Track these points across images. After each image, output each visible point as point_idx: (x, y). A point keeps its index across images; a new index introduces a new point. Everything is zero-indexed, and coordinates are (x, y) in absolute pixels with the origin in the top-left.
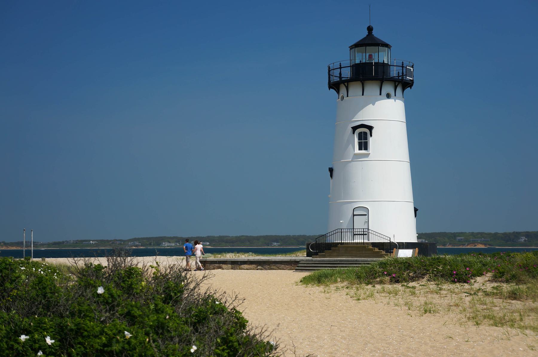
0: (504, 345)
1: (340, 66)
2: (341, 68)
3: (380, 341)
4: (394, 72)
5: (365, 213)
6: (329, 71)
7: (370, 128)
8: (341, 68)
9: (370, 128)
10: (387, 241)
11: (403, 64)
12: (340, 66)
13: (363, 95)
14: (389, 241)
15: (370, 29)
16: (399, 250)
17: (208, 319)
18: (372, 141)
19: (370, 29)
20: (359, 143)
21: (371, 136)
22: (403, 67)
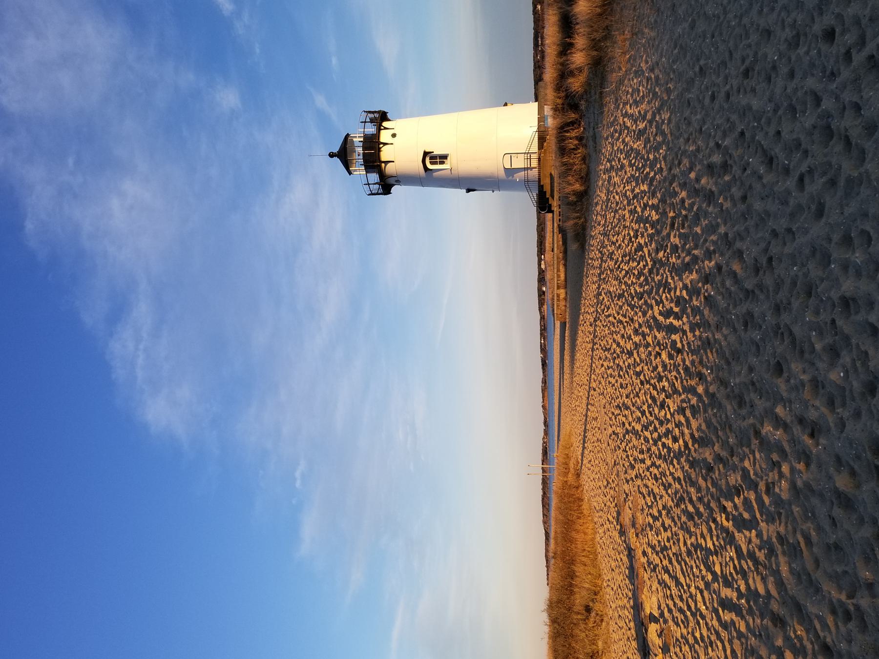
2: (369, 184)
4: (371, 129)
7: (426, 154)
8: (369, 184)
9: (426, 154)
13: (393, 162)
15: (332, 155)
18: (437, 152)
21: (433, 152)
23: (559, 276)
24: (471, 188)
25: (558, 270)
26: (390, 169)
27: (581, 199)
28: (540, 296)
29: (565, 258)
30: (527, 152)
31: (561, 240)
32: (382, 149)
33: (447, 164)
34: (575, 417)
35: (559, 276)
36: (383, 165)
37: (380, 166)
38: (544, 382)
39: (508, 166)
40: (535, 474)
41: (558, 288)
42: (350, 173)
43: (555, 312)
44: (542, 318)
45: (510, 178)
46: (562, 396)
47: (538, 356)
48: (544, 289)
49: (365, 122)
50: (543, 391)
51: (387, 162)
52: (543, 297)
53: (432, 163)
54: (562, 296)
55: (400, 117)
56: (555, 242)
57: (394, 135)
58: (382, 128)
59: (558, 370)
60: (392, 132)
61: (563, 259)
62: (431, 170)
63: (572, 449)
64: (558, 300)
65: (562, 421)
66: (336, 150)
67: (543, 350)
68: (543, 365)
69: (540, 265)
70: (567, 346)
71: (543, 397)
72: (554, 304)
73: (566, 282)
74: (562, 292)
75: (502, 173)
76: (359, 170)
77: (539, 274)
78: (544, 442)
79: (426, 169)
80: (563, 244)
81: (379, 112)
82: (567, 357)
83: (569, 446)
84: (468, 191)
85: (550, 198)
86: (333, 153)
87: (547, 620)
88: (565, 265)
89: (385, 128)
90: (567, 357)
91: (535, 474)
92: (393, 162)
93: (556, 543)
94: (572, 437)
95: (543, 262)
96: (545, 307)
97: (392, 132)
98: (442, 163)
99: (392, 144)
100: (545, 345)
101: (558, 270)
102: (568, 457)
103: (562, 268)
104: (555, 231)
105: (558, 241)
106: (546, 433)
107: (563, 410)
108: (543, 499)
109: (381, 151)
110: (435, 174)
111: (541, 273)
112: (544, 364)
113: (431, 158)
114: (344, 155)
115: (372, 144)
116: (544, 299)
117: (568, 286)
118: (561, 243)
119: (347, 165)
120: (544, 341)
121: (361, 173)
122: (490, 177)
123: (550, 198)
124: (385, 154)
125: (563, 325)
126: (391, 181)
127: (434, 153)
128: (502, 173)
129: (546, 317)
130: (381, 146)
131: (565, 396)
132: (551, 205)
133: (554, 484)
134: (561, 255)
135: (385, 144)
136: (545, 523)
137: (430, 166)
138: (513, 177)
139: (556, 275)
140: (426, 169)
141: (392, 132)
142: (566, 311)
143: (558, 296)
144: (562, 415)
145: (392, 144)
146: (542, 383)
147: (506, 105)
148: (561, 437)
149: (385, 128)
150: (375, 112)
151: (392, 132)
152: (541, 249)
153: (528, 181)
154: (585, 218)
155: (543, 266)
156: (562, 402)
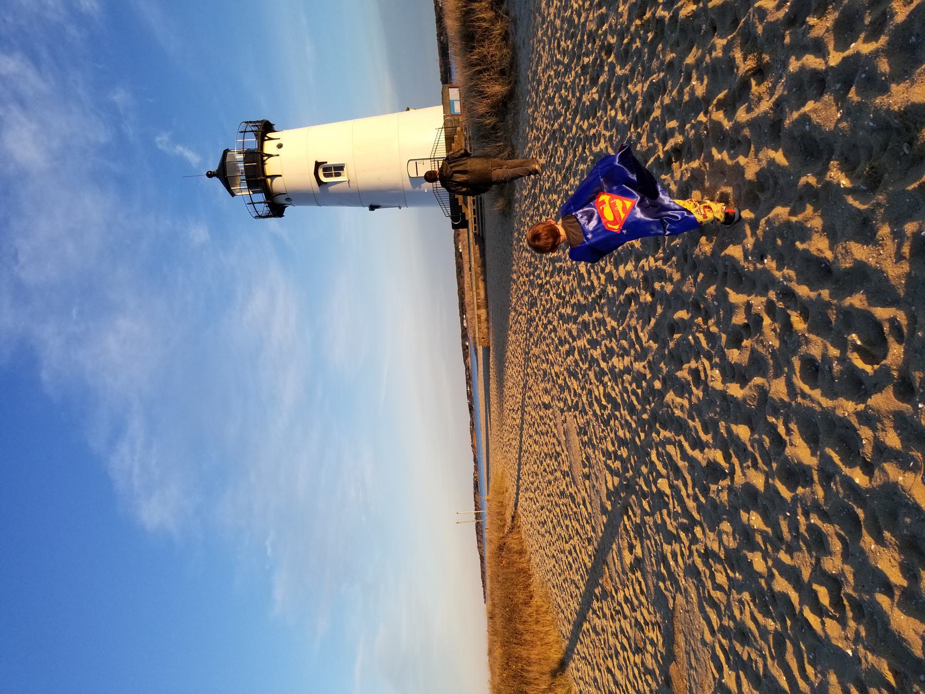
0: (697, 420)
1: (250, 204)
2: (253, 203)
3: (497, 89)
4: (251, 142)
5: (851, 248)
6: (260, 217)
7: (318, 165)
8: (253, 203)
9: (318, 165)
10: (443, 132)
11: (242, 132)
12: (250, 204)
13: (281, 176)
14: (443, 129)
15: (210, 175)
16: (437, 105)
17: (910, 76)
18: (331, 162)
19: (210, 175)
20: (336, 176)
21: (326, 162)
22: (245, 132)
23: (478, 294)
24: (374, 203)
25: (477, 288)
26: (277, 185)
27: (504, 118)
28: (464, 350)
29: (484, 273)
30: (433, 157)
31: (478, 252)
32: (266, 162)
33: (344, 176)
34: (509, 455)
35: (478, 294)
36: (269, 180)
37: (266, 182)
38: (472, 424)
39: (413, 175)
40: (465, 522)
41: (479, 307)
42: (233, 195)
43: (477, 336)
44: (467, 369)
45: (417, 189)
46: (489, 432)
47: (466, 402)
48: (467, 344)
49: (245, 132)
50: (472, 432)
51: (273, 177)
52: (467, 350)
53: (326, 176)
54: (483, 317)
55: (287, 127)
56: (472, 254)
57: (280, 146)
58: (266, 138)
59: (484, 408)
60: (277, 142)
61: (482, 274)
62: (326, 183)
63: (507, 495)
64: (479, 322)
65: (491, 459)
66: (214, 168)
67: (470, 396)
68: (470, 410)
69: (462, 323)
70: (492, 373)
71: (472, 438)
72: (476, 343)
73: (487, 300)
74: (483, 312)
75: (407, 184)
76: (243, 191)
77: (462, 331)
78: (475, 477)
79: (320, 182)
80: (481, 257)
81: (262, 121)
82: (493, 386)
83: (501, 492)
84: (372, 208)
85: (463, 206)
86: (211, 172)
87: (490, 686)
88: (485, 280)
89: (270, 139)
90: (493, 386)
91: (465, 522)
92: (281, 176)
93: (492, 582)
94: (506, 479)
95: (465, 321)
96: (469, 359)
97: (277, 142)
98: (338, 175)
99: (278, 155)
100: (471, 392)
101: (477, 288)
102: (502, 505)
103: (481, 285)
104: (471, 241)
105: (475, 254)
106: (476, 468)
107: (492, 447)
108: (477, 527)
109: (265, 164)
110: (331, 188)
111: (464, 330)
112: (471, 409)
113: (325, 170)
114: (223, 173)
115: (256, 159)
116: (468, 353)
117: (490, 303)
118: (478, 255)
119: (228, 184)
120: (470, 388)
121: (243, 193)
122: (395, 189)
123: (463, 206)
124: (271, 167)
125: (487, 350)
126: (281, 200)
127: (328, 163)
128: (407, 184)
129: (470, 368)
130: (265, 158)
131: (494, 430)
132: (464, 214)
133: (487, 530)
134: (479, 270)
135: (270, 156)
136: (479, 548)
137: (324, 179)
138: (420, 187)
139: (475, 293)
140: (320, 182)
141: (277, 142)
142: (488, 334)
143: (479, 317)
144: (491, 451)
145: (278, 155)
146: (471, 425)
147: (408, 109)
148: (491, 475)
149: (270, 139)
150: (258, 122)
151: (277, 142)
152: (463, 310)
153: (437, 187)
154: (512, 146)
155: (465, 325)
156: (490, 438)
